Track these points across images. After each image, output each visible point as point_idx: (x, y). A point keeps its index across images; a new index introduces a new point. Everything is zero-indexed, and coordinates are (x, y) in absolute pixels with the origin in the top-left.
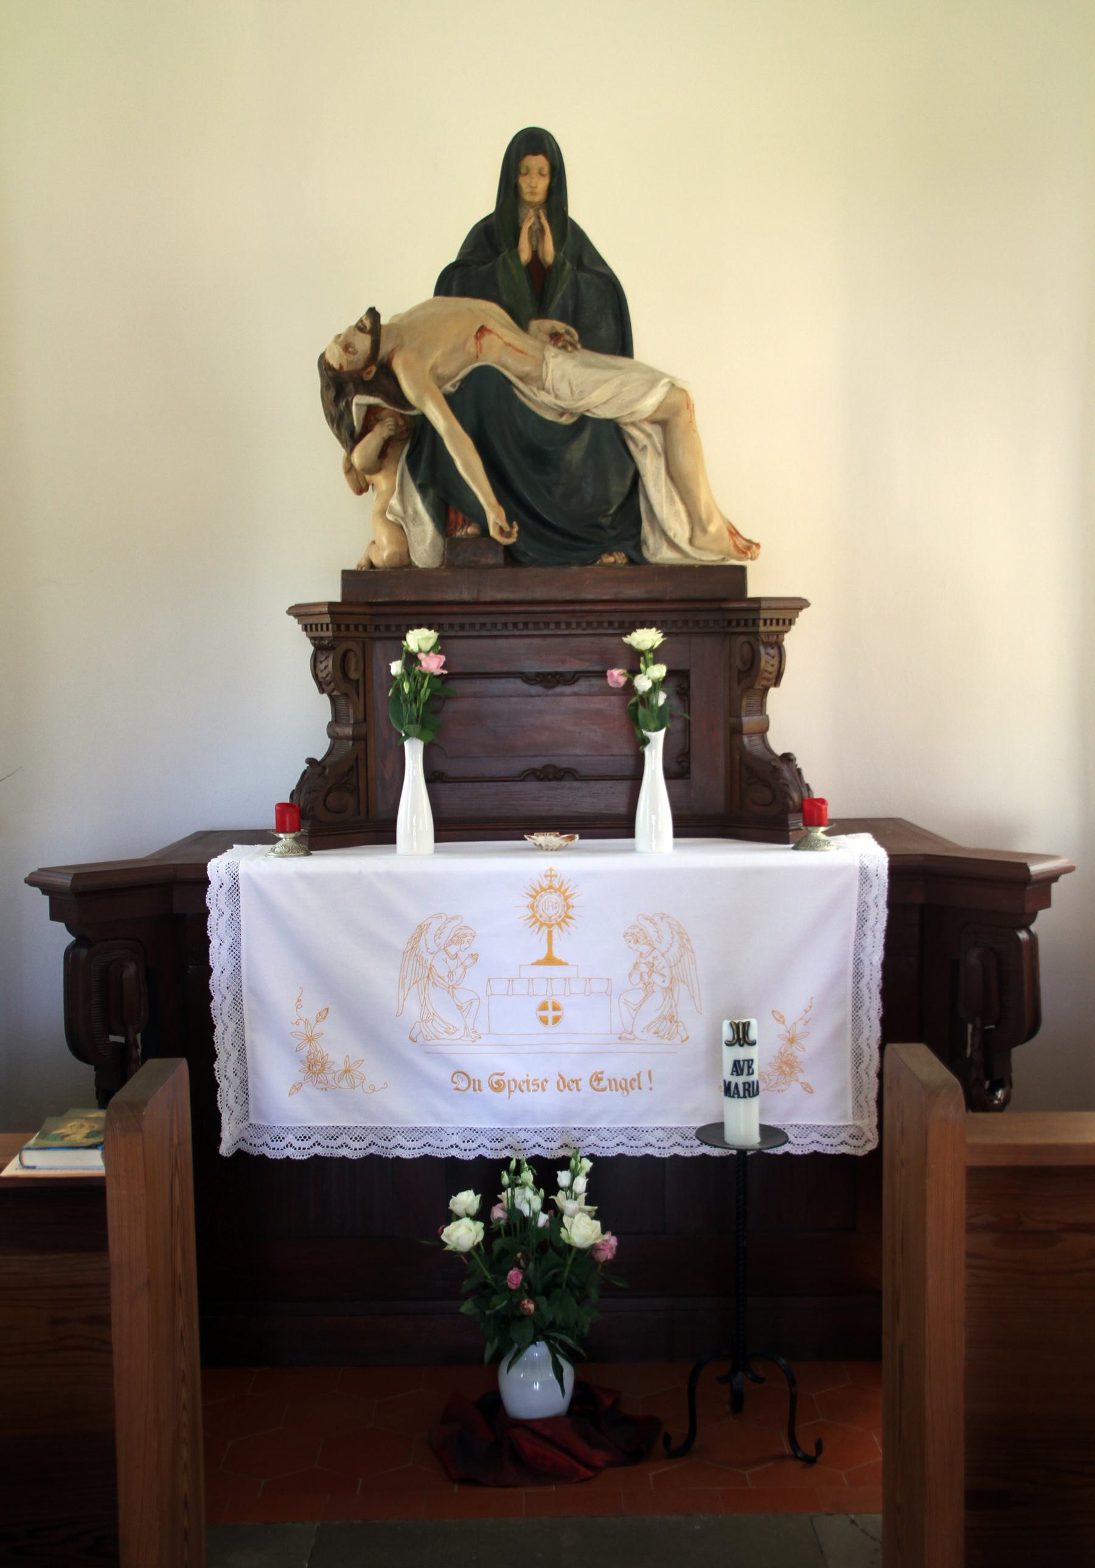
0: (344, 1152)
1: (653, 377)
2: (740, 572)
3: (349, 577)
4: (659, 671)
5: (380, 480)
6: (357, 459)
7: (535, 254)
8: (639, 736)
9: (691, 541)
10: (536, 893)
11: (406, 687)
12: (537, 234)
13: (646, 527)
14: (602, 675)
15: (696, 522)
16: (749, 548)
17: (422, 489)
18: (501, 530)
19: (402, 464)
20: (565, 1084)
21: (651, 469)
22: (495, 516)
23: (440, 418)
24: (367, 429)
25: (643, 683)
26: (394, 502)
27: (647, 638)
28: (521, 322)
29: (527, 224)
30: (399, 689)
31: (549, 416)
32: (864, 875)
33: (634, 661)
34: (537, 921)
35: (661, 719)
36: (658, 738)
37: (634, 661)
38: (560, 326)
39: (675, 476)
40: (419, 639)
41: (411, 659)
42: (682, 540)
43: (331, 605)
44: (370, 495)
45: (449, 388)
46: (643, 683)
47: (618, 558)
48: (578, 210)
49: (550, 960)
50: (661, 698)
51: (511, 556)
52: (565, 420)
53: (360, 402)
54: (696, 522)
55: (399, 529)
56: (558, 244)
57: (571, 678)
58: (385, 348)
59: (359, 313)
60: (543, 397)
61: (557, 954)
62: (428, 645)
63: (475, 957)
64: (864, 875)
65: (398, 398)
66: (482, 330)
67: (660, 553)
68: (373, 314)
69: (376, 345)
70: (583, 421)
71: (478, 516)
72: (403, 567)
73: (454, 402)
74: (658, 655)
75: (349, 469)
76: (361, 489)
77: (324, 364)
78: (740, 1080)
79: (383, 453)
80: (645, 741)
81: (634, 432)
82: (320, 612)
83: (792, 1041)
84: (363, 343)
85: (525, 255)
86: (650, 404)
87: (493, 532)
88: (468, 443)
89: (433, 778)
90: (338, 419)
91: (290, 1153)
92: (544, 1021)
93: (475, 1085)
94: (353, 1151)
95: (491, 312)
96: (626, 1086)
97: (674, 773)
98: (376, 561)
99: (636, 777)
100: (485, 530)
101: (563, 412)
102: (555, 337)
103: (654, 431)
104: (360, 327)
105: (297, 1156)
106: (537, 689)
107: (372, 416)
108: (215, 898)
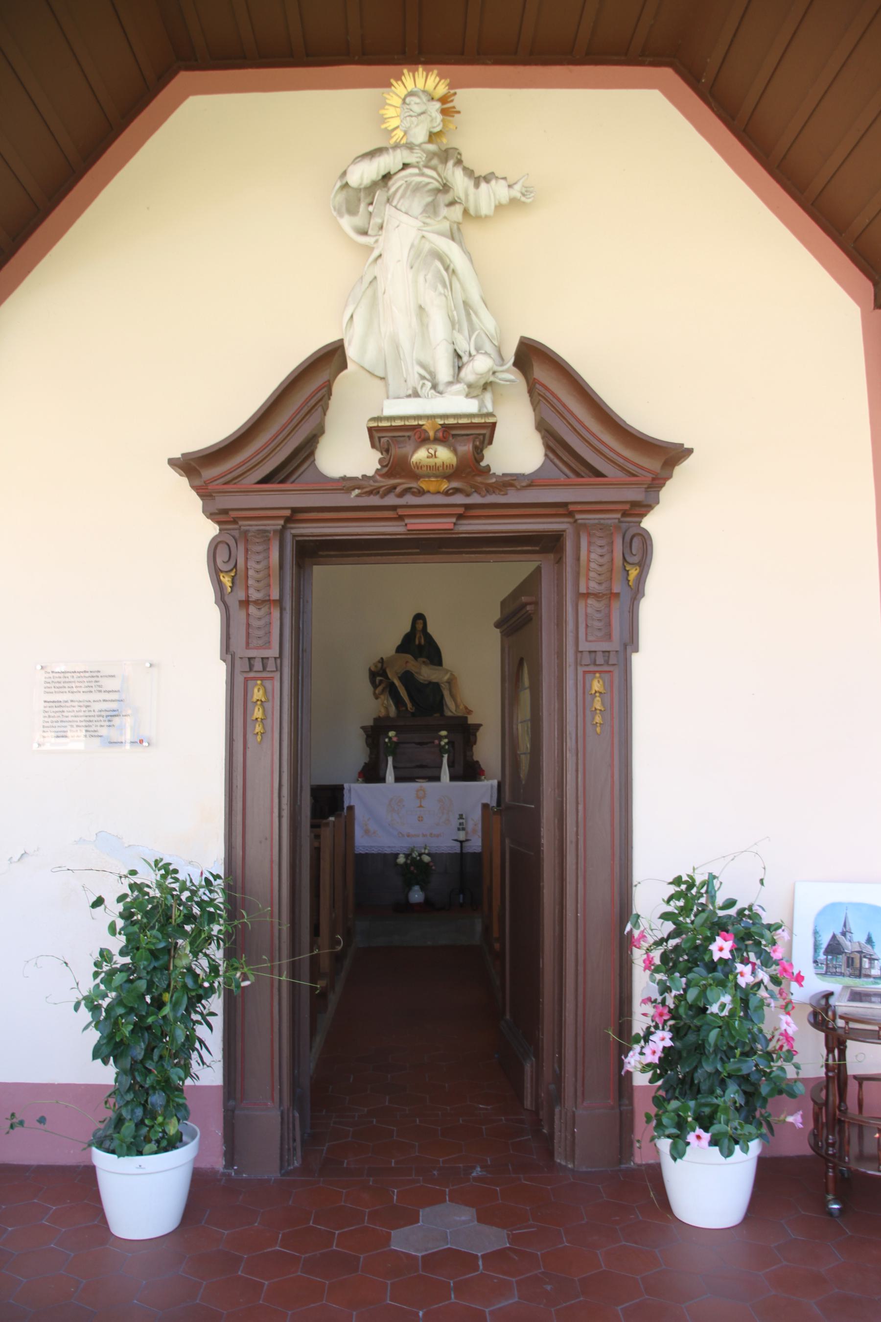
0: (373, 852)
1: (447, 671)
2: (466, 718)
3: (375, 720)
4: (446, 740)
5: (382, 697)
6: (377, 692)
7: (420, 642)
8: (641, 1157)
9: (456, 711)
10: (417, 791)
11: (389, 744)
12: (420, 638)
13: (445, 707)
14: (433, 742)
15: (457, 706)
16: (470, 712)
17: (392, 699)
18: (411, 709)
19: (388, 693)
20: (424, 835)
21: (446, 693)
22: (409, 705)
23: (397, 682)
24: (380, 684)
25: (443, 743)
26: (385, 702)
27: (444, 733)
28: (416, 658)
29: (418, 636)
30: (387, 745)
31: (422, 681)
32: (492, 786)
33: (441, 738)
34: (418, 797)
35: (447, 752)
36: (446, 756)
37: (441, 738)
38: (425, 660)
39: (453, 696)
40: (392, 734)
41: (390, 738)
42: (454, 710)
43: (371, 726)
44: (379, 700)
45: (399, 675)
46: (443, 743)
47: (437, 715)
48: (430, 630)
49: (421, 806)
50: (447, 747)
51: (413, 715)
52: (426, 683)
53: (378, 679)
54: (457, 706)
55: (387, 709)
56: (425, 640)
57: (427, 743)
58: (385, 666)
59: (379, 658)
60: (422, 677)
61: (422, 805)
62: (394, 735)
63: (404, 806)
64: (492, 786)
65: (387, 677)
66: (407, 662)
67: (448, 713)
68: (382, 659)
69: (382, 666)
70: (430, 683)
71: (405, 705)
72: (387, 718)
73: (401, 679)
74: (446, 737)
75: (374, 693)
76: (377, 698)
77: (370, 670)
78: (461, 827)
79: (383, 692)
80: (443, 757)
81: (443, 685)
82: (282, 817)
83: (476, 825)
84: (379, 665)
85: (417, 642)
86: (446, 678)
87: (409, 709)
88: (403, 688)
89: (395, 767)
90: (373, 682)
91: (361, 852)
92: (419, 820)
93: (403, 835)
94: (375, 851)
95: (409, 657)
96: (438, 836)
97: (451, 765)
98: (381, 716)
99: (440, 767)
100: (407, 708)
101: (425, 680)
102: (424, 662)
103: (447, 684)
104: (379, 662)
105: (362, 852)
106: (419, 746)
107: (381, 682)
108: (346, 792)
